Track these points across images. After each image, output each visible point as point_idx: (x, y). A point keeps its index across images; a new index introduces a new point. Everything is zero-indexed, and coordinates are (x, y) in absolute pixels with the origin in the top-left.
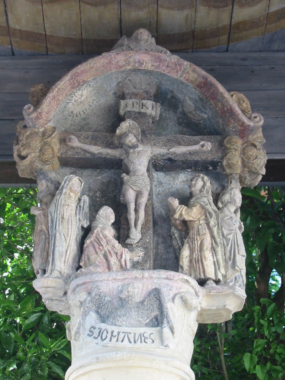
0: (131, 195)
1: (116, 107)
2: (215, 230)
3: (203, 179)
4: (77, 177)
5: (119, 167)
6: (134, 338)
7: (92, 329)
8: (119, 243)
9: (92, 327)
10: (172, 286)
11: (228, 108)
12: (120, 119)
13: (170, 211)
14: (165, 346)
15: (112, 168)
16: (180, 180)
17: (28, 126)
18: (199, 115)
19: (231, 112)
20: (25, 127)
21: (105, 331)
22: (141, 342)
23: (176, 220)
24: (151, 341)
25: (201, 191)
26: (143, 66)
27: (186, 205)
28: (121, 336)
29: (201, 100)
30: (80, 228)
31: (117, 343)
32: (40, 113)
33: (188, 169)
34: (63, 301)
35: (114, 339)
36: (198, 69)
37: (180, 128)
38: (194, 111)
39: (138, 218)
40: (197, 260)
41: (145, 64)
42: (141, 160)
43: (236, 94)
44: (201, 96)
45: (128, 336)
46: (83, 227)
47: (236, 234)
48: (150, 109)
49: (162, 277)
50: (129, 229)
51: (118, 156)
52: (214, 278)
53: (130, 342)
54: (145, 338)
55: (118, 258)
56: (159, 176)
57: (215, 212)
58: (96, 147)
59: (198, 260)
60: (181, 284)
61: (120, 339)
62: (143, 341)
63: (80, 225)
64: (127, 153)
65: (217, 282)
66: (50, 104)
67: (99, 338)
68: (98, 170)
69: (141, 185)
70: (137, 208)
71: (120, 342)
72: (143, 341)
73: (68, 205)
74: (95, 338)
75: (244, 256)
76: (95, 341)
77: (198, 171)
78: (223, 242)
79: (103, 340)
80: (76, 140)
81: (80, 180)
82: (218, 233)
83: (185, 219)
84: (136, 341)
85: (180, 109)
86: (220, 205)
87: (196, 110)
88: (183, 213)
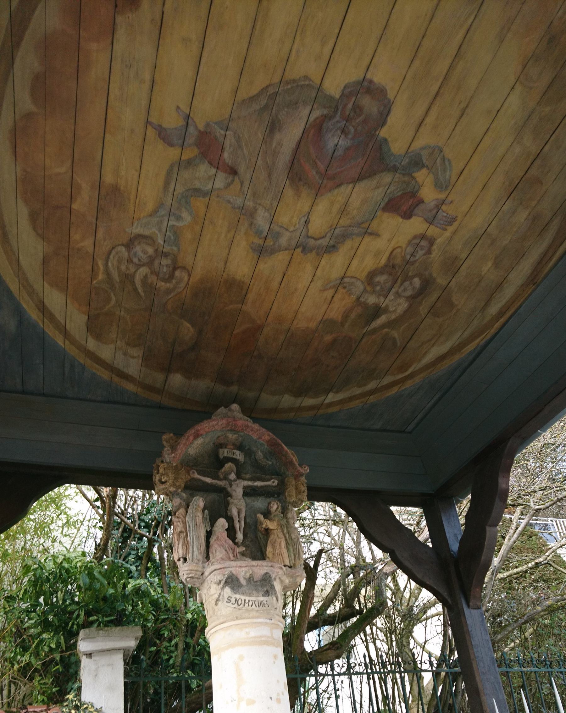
0: (234, 512)
1: (217, 455)
2: (287, 536)
3: (277, 504)
5: (224, 494)
9: (229, 597)
13: (256, 523)
16: (260, 503)
18: (266, 462)
19: (291, 462)
25: (276, 511)
28: (251, 603)
35: (247, 605)
36: (270, 433)
39: (239, 526)
42: (238, 490)
52: (289, 565)
58: (209, 479)
60: (277, 570)
61: (250, 605)
64: (231, 485)
67: (236, 604)
69: (238, 505)
71: (250, 607)
85: (253, 457)
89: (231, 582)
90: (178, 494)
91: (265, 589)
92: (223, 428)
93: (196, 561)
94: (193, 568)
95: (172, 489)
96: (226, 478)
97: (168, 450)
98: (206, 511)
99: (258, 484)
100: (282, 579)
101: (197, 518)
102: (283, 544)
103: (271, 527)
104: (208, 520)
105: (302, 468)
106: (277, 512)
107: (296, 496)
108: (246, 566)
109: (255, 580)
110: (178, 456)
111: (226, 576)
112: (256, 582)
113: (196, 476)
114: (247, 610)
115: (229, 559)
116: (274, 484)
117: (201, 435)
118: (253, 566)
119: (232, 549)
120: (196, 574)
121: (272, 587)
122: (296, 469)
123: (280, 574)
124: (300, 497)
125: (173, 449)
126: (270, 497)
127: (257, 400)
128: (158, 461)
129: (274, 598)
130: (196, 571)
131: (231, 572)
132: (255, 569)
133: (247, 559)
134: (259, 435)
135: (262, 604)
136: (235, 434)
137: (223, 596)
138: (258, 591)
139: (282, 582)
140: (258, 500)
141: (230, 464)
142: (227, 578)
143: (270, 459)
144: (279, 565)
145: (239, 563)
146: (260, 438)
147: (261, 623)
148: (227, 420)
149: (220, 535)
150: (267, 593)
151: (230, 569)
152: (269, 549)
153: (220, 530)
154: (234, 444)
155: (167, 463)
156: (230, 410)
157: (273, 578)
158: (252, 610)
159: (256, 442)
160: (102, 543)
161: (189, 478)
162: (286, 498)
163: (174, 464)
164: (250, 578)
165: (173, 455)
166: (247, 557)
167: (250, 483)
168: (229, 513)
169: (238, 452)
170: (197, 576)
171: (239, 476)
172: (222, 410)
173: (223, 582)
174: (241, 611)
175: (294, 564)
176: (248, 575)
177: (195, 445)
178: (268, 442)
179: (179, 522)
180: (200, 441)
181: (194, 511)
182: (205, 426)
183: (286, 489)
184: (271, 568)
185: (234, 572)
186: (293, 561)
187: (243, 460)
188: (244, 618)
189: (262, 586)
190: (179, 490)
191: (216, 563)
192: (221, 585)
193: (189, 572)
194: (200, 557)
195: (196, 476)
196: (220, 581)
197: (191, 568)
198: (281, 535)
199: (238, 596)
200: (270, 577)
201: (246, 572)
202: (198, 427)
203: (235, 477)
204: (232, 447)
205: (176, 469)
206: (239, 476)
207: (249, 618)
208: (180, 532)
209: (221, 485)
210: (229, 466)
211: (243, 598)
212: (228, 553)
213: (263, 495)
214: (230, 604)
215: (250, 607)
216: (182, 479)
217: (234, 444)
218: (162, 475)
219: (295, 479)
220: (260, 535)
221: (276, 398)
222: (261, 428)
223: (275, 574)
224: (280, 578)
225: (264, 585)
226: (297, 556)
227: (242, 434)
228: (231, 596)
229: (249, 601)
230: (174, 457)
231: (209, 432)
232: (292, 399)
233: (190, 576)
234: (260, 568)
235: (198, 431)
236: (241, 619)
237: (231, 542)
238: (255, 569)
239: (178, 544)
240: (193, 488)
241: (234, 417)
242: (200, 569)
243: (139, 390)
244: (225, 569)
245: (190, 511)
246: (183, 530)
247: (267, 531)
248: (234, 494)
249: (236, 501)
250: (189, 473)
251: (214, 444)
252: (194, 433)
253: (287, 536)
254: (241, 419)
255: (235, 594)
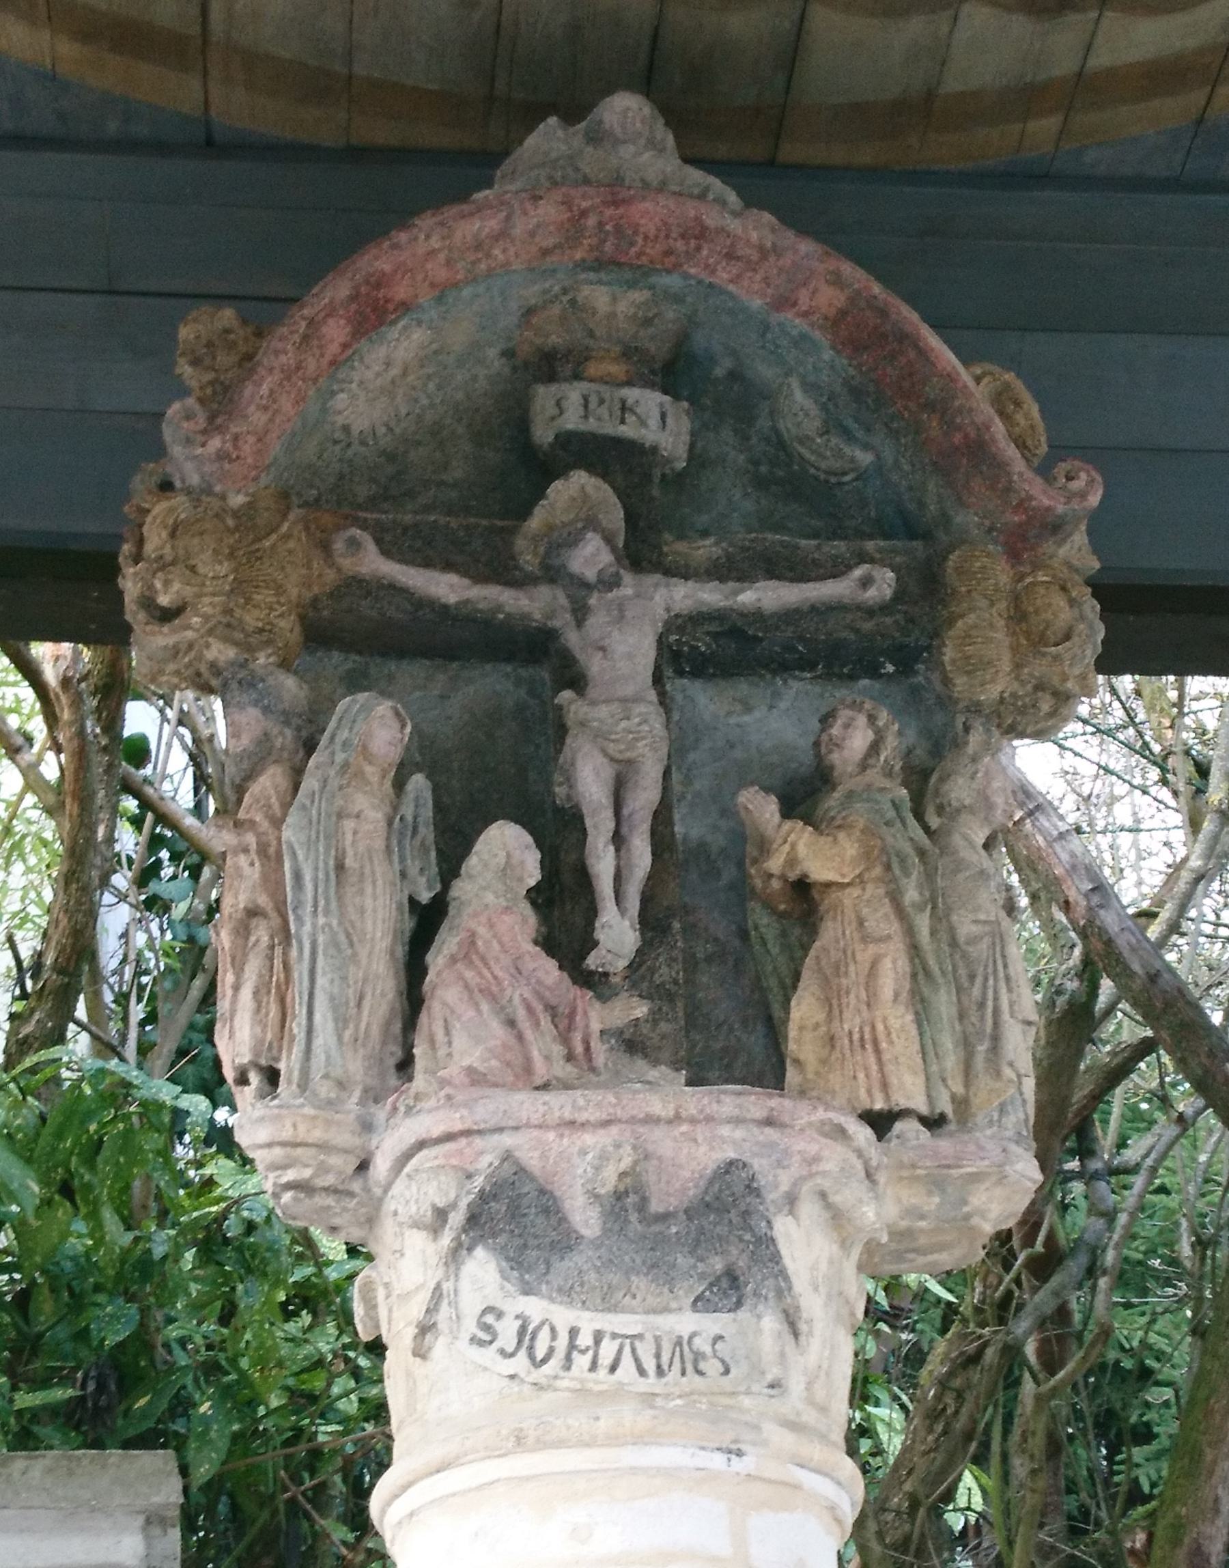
0: (590, 782)
1: (519, 421)
2: (923, 923)
3: (872, 719)
4: (390, 703)
5: (545, 659)
6: (658, 1356)
7: (489, 1319)
8: (561, 968)
9: (489, 1310)
10: (786, 1152)
11: (966, 436)
12: (539, 467)
13: (744, 845)
14: (772, 1386)
15: (509, 659)
16: (775, 718)
17: (178, 484)
18: (839, 454)
19: (978, 450)
20: (166, 486)
21: (546, 1328)
22: (683, 1373)
23: (771, 876)
24: (722, 1370)
25: (864, 766)
26: (633, 250)
27: (808, 820)
28: (608, 1350)
29: (857, 393)
30: (406, 902)
31: (593, 1375)
32: (236, 438)
33: (803, 669)
34: (351, 1194)
35: (582, 1362)
36: (848, 269)
37: (763, 502)
38: (821, 435)
39: (616, 866)
40: (856, 1037)
41: (640, 240)
42: (622, 643)
43: (991, 373)
44: (501, 257)
45: (634, 1350)
46: (413, 901)
47: (1002, 940)
48: (654, 422)
49: (749, 1116)
50: (592, 912)
51: (537, 616)
52: (924, 1109)
53: (642, 1372)
54: (698, 1356)
55: (561, 1027)
56: (706, 700)
57: (922, 853)
58: (453, 578)
59: (862, 1039)
60: (810, 1145)
62: (689, 1368)
63: (406, 893)
64: (580, 613)
65: (934, 1123)
66: (275, 402)
68: (455, 665)
69: (615, 747)
70: (624, 830)
71: (602, 1373)
72: (689, 1368)
73: (358, 816)
74: (502, 1352)
75: (1029, 1023)
76: (510, 1366)
77: (840, 677)
78: (955, 970)
79: (538, 1364)
80: (371, 547)
81: (397, 714)
82: (933, 933)
83: (806, 876)
84: (665, 1367)
85: (763, 423)
86: (934, 822)
87: (827, 432)
88: (802, 850)
89: (509, 1216)
90: (249, 683)
91: (718, 1264)
92: (545, 252)
93: (325, 1090)
94: (302, 1135)
95: (220, 652)
96: (552, 573)
97: (189, 417)
98: (418, 782)
99: (766, 596)
100: (836, 1199)
101: (349, 825)
102: (893, 972)
103: (820, 871)
104: (427, 833)
105: (1049, 479)
106: (874, 776)
107: (1018, 666)
108: (606, 1123)
109: (655, 1207)
110: (248, 447)
111: (479, 1181)
112: (664, 1217)
113: (373, 563)
114: (581, 1392)
115: (525, 1076)
116: (871, 594)
117: (405, 307)
118: (651, 1120)
119: (552, 1010)
120: (323, 1169)
121: (765, 1251)
122: (1008, 489)
123: (829, 1166)
124: (1038, 668)
125: (220, 403)
126: (852, 677)
127: (792, 51)
128: (141, 484)
129: (770, 1323)
130: (322, 1147)
131: (507, 1156)
132: (663, 1142)
133: (653, 1074)
134: (775, 284)
135: (688, 1358)
136: (632, 285)
137: (454, 1304)
138: (661, 1271)
139: (837, 1218)
140: (776, 695)
141: (580, 479)
142: (484, 1197)
143: (860, 434)
144: (821, 1114)
145: (559, 1104)
146: (783, 302)
147: (669, 1474)
148: (567, 203)
149: (482, 931)
150: (728, 1290)
151: (507, 1140)
152: (804, 1009)
153: (490, 898)
154: (628, 353)
155: (188, 491)
156: (596, 137)
157: (771, 1196)
158: (617, 1394)
159: (766, 328)
160: (49, 961)
161: (331, 576)
162: (947, 681)
163: (237, 500)
164: (619, 1196)
165: (215, 443)
166: (656, 1063)
167: (711, 595)
168: (560, 791)
169: (649, 401)
170: (329, 1180)
171: (641, 552)
172: (549, 138)
173: (457, 1218)
174: (548, 1396)
175: (962, 1104)
176: (609, 1179)
177: (382, 363)
178: (836, 321)
179: (246, 850)
180: (403, 344)
181: (334, 783)
182: (421, 248)
183: (951, 622)
184: (771, 1133)
185: (531, 1159)
186: (959, 1089)
187: (682, 451)
188: (560, 1444)
189: (698, 1244)
190: (262, 659)
191: (432, 1103)
192: (446, 1239)
193: (278, 1152)
194: (356, 1067)
195: (373, 563)
196: (441, 1215)
197: (287, 1134)
198: (881, 920)
199: (535, 1308)
200: (752, 1189)
201: (604, 1157)
202: (377, 260)
203: (606, 558)
204: (617, 369)
205: (245, 532)
206: (641, 552)
207: (589, 1443)
208: (253, 912)
209: (526, 617)
210: (574, 488)
211: (563, 1316)
212: (520, 1037)
213: (806, 664)
214: (488, 1355)
215: (602, 1373)
216: (280, 590)
217: (628, 353)
218: (162, 565)
219: (1014, 555)
220: (762, 920)
221: (915, 27)
222: (789, 236)
223: (796, 1168)
224: (823, 1195)
225: (715, 1240)
226: (982, 1048)
227: (672, 281)
228: (498, 1304)
229: (598, 1337)
230: (222, 456)
231: (456, 285)
232: (1020, 25)
233: (290, 1175)
234: (699, 1131)
235: (380, 282)
236: (542, 1445)
237: (549, 970)
238: (663, 1142)
239: (237, 988)
240: (354, 638)
241: (618, 180)
242: (345, 1138)
243: (67, 49)
244: (478, 1142)
245: (310, 783)
246: (263, 901)
247: (803, 890)
248: (595, 666)
249: (603, 711)
250: (325, 547)
251: (508, 354)
252: (354, 298)
253: (923, 923)
254: (662, 187)
255: (527, 1290)
